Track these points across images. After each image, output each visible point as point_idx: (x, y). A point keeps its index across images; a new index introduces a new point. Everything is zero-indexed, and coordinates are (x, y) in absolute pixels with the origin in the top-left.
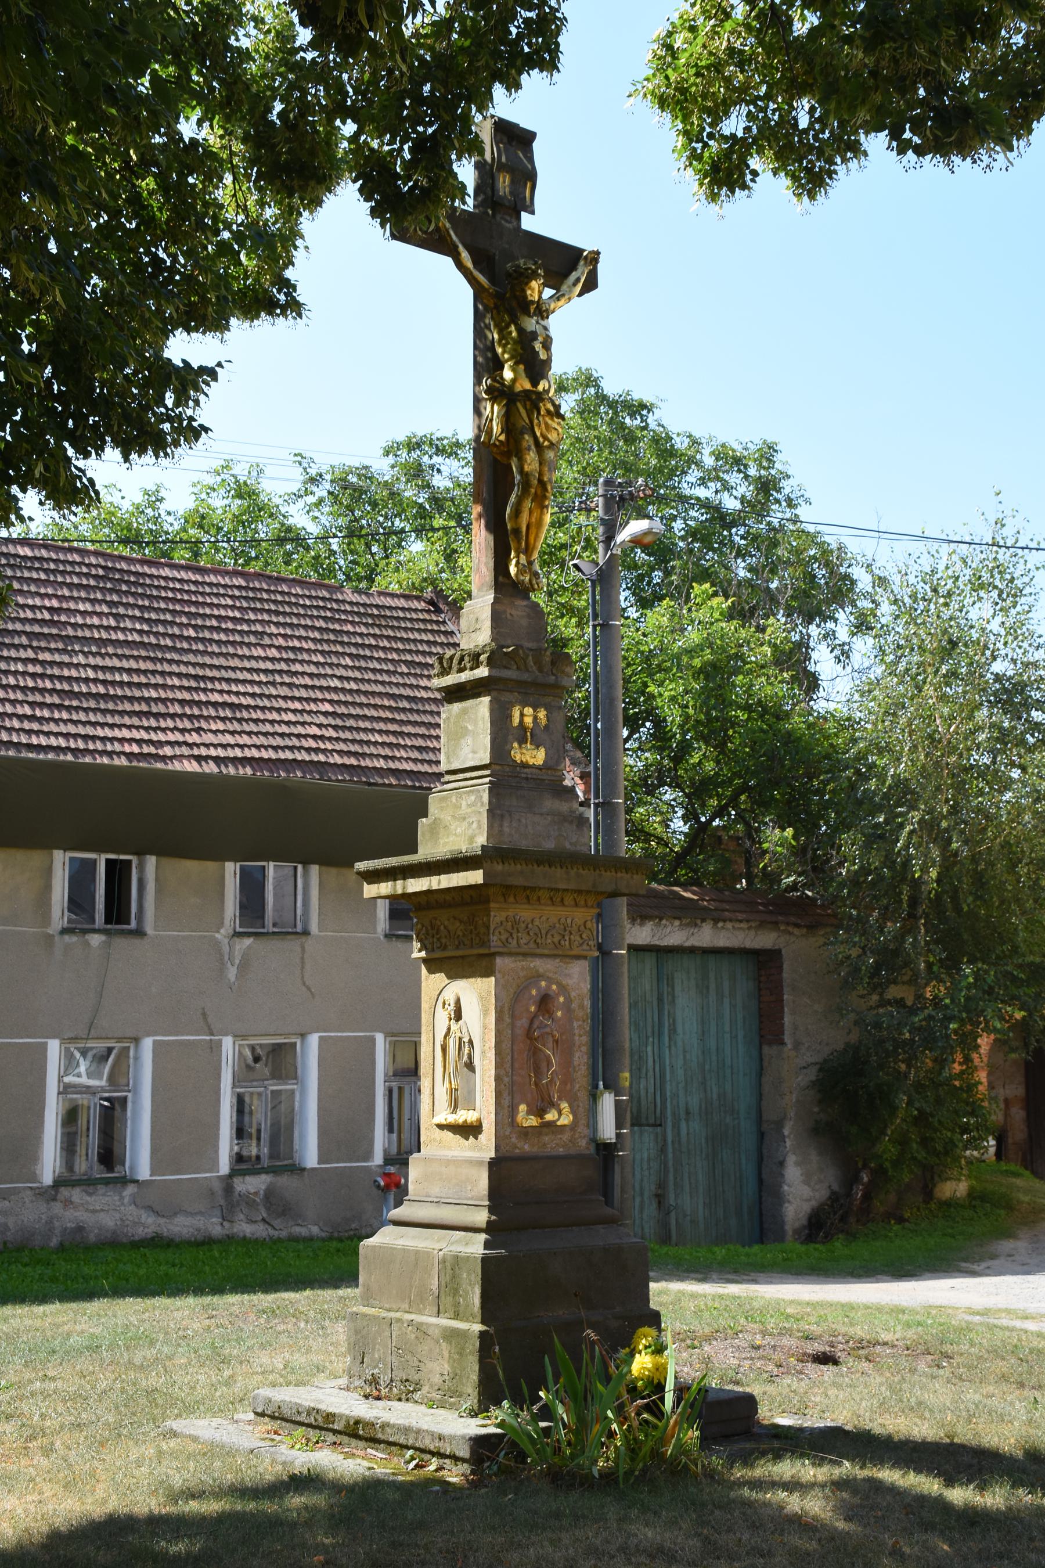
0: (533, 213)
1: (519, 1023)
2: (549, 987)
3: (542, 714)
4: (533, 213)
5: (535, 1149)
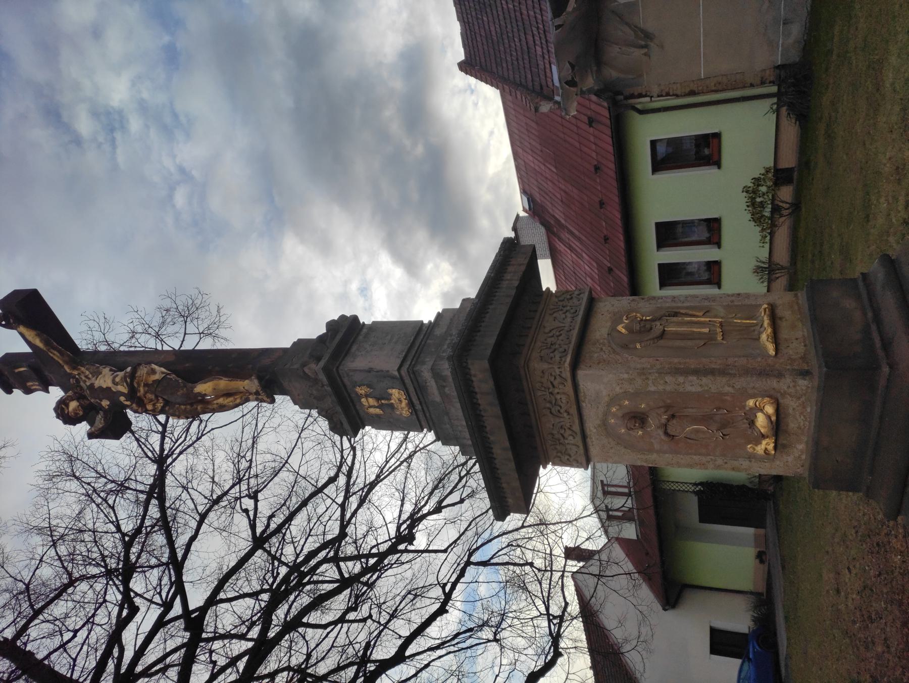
1: (657, 446)
2: (614, 415)
5: (805, 439)
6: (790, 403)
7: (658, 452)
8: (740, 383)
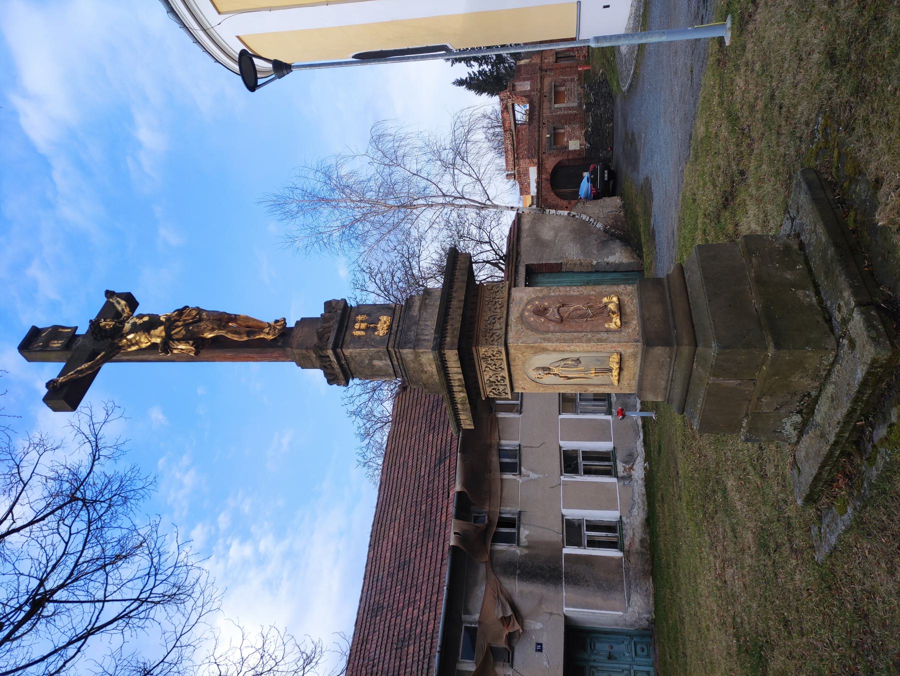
0: (76, 328)
1: (552, 328)
2: (528, 311)
3: (359, 318)
4: (76, 328)
5: (636, 317)
6: (626, 299)
7: (553, 332)
8: (598, 289)
